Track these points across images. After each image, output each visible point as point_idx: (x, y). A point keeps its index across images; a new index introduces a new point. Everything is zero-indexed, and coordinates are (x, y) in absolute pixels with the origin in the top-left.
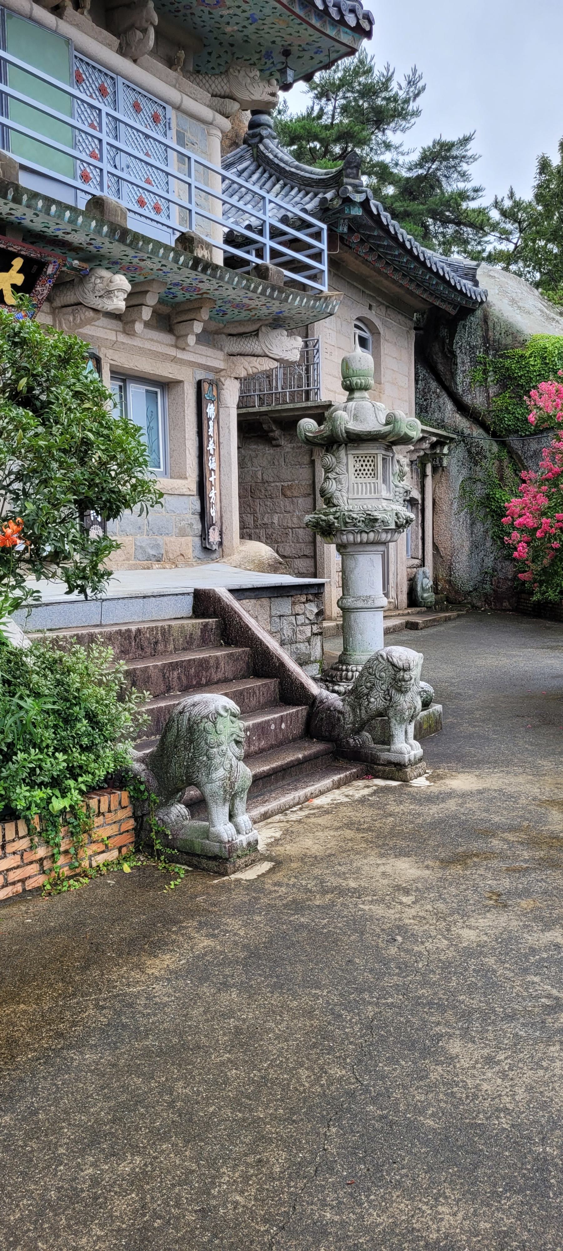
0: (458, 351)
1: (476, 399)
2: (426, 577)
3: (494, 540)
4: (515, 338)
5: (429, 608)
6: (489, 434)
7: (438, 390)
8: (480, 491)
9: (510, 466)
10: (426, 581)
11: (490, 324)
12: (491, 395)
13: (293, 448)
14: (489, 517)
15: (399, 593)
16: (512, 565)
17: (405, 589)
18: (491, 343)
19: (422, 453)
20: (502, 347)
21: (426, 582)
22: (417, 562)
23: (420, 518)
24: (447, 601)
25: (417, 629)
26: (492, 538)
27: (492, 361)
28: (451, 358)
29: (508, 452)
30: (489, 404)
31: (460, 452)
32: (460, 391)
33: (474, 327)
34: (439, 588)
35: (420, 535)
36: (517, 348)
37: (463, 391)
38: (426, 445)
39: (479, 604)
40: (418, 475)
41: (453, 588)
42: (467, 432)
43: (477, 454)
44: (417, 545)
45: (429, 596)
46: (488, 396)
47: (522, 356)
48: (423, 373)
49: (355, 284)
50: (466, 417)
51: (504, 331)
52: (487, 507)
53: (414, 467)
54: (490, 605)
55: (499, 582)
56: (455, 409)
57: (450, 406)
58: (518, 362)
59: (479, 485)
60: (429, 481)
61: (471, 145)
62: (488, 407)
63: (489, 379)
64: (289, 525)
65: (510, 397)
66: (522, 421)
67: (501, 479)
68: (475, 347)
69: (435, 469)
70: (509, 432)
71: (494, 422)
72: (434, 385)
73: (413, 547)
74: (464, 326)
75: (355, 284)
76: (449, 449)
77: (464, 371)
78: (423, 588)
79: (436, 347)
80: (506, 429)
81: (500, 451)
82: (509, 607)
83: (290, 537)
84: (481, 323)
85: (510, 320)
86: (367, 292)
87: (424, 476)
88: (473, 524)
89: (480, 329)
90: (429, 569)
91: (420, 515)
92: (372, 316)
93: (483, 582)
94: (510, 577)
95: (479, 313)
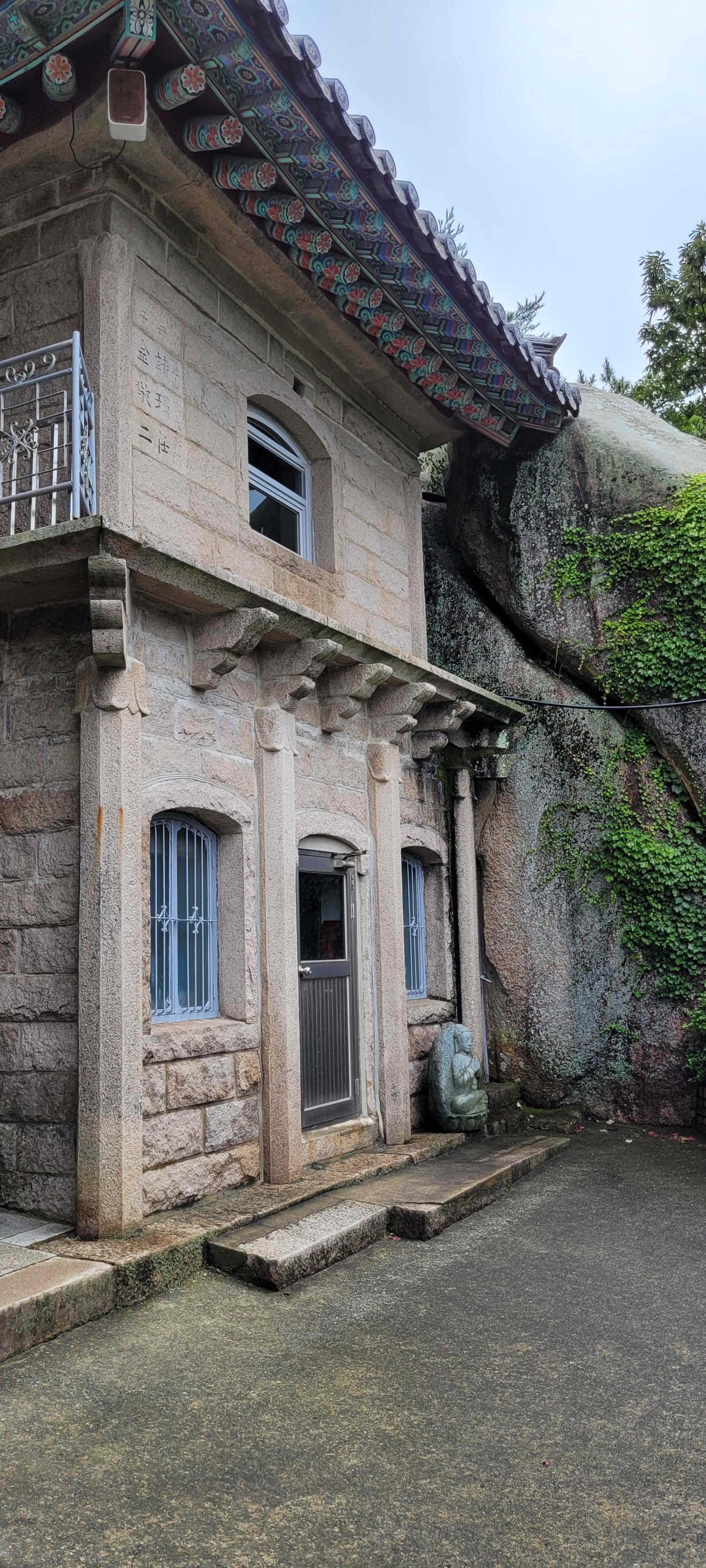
0: (521, 525)
1: (568, 628)
2: (463, 1050)
3: (629, 952)
4: (648, 487)
5: (474, 1134)
6: (600, 702)
7: (481, 615)
8: (588, 835)
9: (655, 773)
10: (462, 1060)
11: (590, 461)
12: (601, 615)
13: (32, 688)
14: (613, 895)
15: (388, 1097)
16: (675, 1014)
17: (405, 1082)
18: (594, 500)
19: (442, 741)
20: (619, 507)
21: (464, 1060)
22: (440, 1008)
23: (446, 900)
24: (523, 1099)
25: (422, 1236)
26: (624, 946)
27: (598, 540)
28: (505, 542)
29: (649, 743)
30: (596, 635)
31: (537, 747)
32: (530, 611)
33: (553, 470)
34: (503, 1066)
35: (448, 940)
36: (654, 505)
37: (537, 610)
38: (451, 721)
39: (601, 1109)
40: (437, 796)
41: (536, 1068)
42: (551, 699)
43: (576, 749)
44: (440, 966)
45: (470, 1101)
46: (594, 619)
47: (666, 523)
48: (446, 580)
49: (246, 308)
50: (546, 670)
51: (621, 472)
52: (607, 872)
53: (426, 776)
54: (627, 1111)
55: (646, 1056)
56: (520, 652)
57: (508, 647)
58: (658, 536)
59: (584, 821)
60: (465, 812)
61: (539, 317)
62: (596, 642)
63: (594, 581)
64: (14, 917)
65: (646, 617)
66: (680, 666)
67: (637, 804)
68: (560, 512)
69: (479, 786)
70: (652, 692)
71: (612, 676)
72: (471, 604)
73: (432, 970)
74: (532, 472)
75: (246, 308)
76: (510, 738)
77: (537, 568)
78: (454, 1080)
79: (473, 523)
80: (640, 689)
81: (628, 741)
82: (675, 1118)
83: (16, 955)
84: (571, 461)
85: (635, 449)
86: (287, 345)
87: (452, 799)
88: (575, 913)
89: (567, 474)
90: (473, 1028)
91: (446, 892)
92: (305, 407)
93: (607, 1053)
94: (673, 1043)
95: (563, 441)
